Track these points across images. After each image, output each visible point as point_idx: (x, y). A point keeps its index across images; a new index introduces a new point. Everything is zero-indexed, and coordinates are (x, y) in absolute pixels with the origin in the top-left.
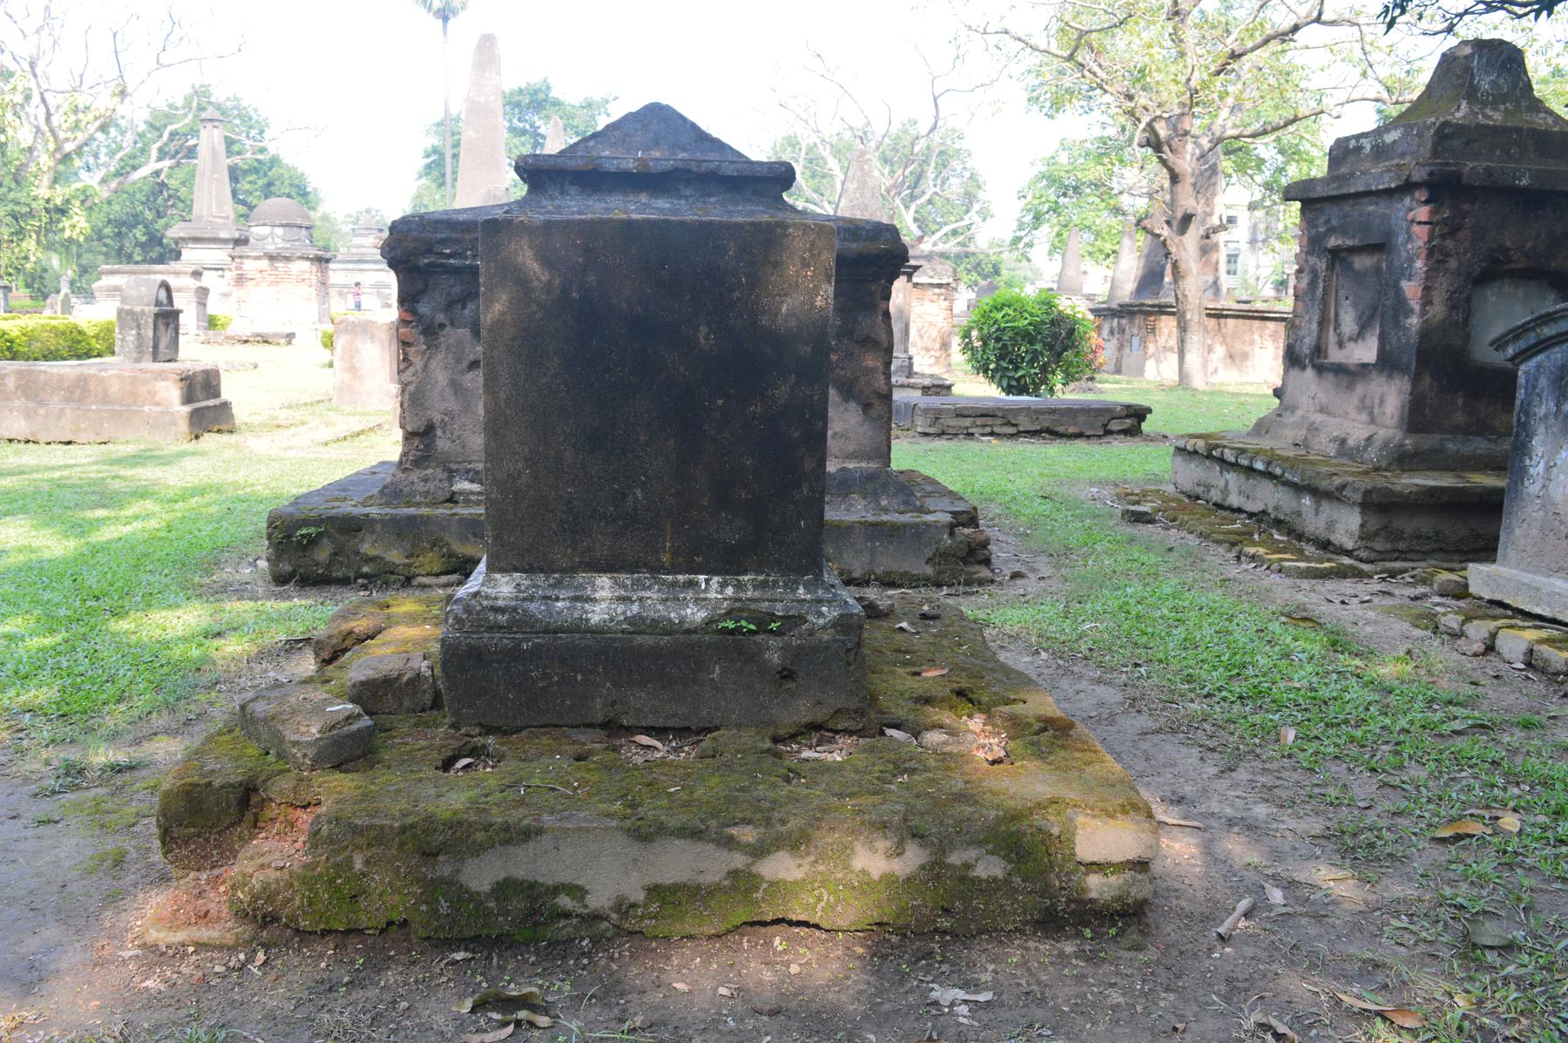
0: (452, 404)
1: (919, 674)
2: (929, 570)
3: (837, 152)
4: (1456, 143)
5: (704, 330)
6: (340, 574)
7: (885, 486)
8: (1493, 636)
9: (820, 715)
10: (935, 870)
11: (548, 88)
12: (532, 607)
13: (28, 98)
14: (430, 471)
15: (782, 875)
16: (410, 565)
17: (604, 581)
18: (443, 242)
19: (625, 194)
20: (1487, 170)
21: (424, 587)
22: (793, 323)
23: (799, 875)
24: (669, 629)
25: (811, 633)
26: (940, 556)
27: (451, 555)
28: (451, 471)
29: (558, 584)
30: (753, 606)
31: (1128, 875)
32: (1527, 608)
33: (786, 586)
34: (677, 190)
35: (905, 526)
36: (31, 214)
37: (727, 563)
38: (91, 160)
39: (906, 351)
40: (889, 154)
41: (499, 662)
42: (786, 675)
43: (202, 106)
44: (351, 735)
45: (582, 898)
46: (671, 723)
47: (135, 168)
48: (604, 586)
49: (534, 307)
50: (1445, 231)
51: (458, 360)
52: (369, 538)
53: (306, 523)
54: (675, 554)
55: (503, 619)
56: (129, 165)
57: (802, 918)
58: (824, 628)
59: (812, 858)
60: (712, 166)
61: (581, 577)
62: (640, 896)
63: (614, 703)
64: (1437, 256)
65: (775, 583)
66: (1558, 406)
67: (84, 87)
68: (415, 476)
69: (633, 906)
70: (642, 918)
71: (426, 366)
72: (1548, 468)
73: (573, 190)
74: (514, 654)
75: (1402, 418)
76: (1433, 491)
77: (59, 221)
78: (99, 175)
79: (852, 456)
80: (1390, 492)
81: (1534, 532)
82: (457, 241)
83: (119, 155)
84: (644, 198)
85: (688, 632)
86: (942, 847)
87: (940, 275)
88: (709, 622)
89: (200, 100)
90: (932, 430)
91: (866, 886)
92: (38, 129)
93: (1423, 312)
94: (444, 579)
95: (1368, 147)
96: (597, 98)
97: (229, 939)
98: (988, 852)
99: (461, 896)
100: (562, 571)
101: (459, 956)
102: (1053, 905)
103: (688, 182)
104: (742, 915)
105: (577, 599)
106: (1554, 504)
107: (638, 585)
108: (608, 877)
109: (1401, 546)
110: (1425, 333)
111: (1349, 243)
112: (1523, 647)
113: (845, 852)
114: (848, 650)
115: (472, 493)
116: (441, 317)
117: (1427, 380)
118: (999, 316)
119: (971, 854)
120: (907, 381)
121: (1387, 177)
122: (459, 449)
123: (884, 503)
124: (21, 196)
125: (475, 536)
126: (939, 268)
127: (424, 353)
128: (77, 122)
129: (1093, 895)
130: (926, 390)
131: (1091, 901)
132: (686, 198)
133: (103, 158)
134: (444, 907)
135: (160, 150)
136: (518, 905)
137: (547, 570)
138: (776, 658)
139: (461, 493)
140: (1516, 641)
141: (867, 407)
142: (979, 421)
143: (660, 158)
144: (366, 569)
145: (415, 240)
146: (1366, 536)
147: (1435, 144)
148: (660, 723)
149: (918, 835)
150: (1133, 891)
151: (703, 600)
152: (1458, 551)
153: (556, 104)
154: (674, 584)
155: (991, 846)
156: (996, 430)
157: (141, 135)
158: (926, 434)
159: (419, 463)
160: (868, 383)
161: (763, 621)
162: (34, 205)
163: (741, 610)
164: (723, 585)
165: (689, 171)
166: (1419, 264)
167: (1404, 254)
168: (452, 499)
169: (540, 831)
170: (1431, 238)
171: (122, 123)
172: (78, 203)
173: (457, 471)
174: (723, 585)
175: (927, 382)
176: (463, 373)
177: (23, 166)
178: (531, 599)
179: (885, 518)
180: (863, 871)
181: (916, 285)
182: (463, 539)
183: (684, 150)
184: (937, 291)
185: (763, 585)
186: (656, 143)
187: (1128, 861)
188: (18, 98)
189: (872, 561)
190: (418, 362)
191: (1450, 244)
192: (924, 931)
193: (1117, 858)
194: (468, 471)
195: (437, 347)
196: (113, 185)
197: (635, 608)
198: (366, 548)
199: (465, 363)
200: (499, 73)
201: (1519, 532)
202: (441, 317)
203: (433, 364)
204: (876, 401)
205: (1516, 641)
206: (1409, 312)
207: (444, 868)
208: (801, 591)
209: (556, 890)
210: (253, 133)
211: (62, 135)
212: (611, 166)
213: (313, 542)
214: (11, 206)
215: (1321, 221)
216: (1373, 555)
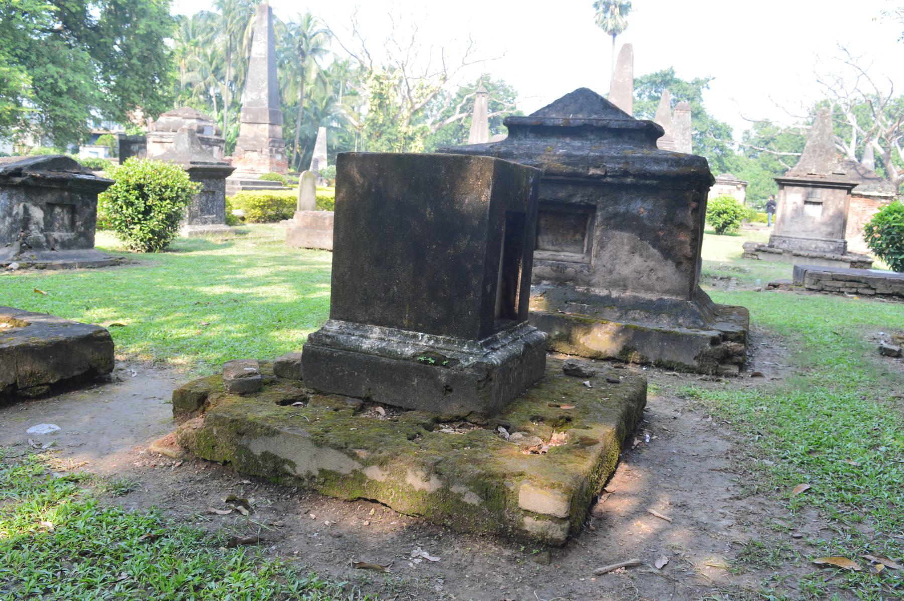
1: (559, 406)
2: (695, 364)
3: (855, 110)
5: (429, 210)
7: (684, 311)
9: (463, 412)
10: (444, 493)
11: (673, 73)
12: (341, 337)
13: (401, 82)
15: (375, 478)
17: (377, 329)
19: (558, 138)
22: (470, 209)
24: (397, 357)
26: (703, 356)
29: (357, 329)
30: (438, 351)
31: (548, 523)
33: (459, 343)
34: (586, 136)
35: (683, 335)
36: (397, 140)
37: (433, 329)
38: (429, 113)
39: (843, 238)
40: (893, 111)
42: (448, 389)
43: (487, 86)
44: (249, 382)
45: (294, 468)
46: (394, 403)
47: (449, 117)
48: (376, 332)
54: (410, 321)
55: (328, 341)
56: (447, 115)
57: (383, 502)
58: (467, 367)
59: (388, 472)
60: (605, 122)
61: (368, 326)
62: (316, 473)
63: (369, 389)
65: (454, 341)
67: (427, 77)
69: (314, 477)
70: (317, 483)
73: (531, 135)
74: (330, 358)
77: (410, 144)
78: (430, 121)
79: (667, 292)
83: (442, 110)
84: (568, 140)
85: (404, 359)
86: (448, 482)
87: (887, 191)
88: (415, 356)
89: (485, 81)
90: (814, 287)
91: (412, 493)
92: (404, 97)
96: (702, 78)
97: (174, 455)
98: (470, 490)
99: (249, 455)
100: (360, 322)
101: (245, 482)
102: (505, 528)
103: (592, 132)
104: (357, 494)
105: (362, 336)
107: (392, 334)
108: (305, 461)
113: (403, 473)
114: (479, 381)
118: (891, 218)
119: (462, 489)
120: (840, 257)
123: (680, 321)
124: (393, 130)
126: (886, 186)
128: (422, 94)
129: (528, 528)
130: (853, 264)
131: (527, 532)
132: (591, 140)
133: (435, 112)
134: (244, 460)
135: (462, 108)
136: (270, 465)
137: (354, 320)
138: (443, 379)
141: (678, 264)
142: (848, 284)
143: (581, 118)
148: (389, 402)
149: (439, 474)
150: (550, 532)
151: (414, 345)
153: (678, 82)
154: (407, 335)
155: (472, 487)
156: (860, 291)
157: (454, 100)
158: (810, 289)
160: (680, 250)
161: (439, 361)
162: (399, 135)
163: (432, 352)
164: (429, 339)
165: (592, 126)
169: (279, 433)
171: (445, 94)
172: (419, 135)
174: (429, 339)
175: (855, 259)
177: (396, 116)
178: (342, 333)
179: (677, 330)
180: (411, 485)
181: (853, 195)
183: (596, 114)
184: (884, 201)
185: (448, 342)
186: (581, 110)
187: (549, 515)
188: (396, 82)
189: (661, 354)
192: (438, 523)
193: (541, 511)
196: (437, 126)
197: (384, 344)
200: (632, 66)
204: (685, 261)
207: (244, 441)
208: (466, 347)
209: (285, 461)
210: (510, 99)
211: (415, 100)
212: (549, 123)
214: (388, 136)
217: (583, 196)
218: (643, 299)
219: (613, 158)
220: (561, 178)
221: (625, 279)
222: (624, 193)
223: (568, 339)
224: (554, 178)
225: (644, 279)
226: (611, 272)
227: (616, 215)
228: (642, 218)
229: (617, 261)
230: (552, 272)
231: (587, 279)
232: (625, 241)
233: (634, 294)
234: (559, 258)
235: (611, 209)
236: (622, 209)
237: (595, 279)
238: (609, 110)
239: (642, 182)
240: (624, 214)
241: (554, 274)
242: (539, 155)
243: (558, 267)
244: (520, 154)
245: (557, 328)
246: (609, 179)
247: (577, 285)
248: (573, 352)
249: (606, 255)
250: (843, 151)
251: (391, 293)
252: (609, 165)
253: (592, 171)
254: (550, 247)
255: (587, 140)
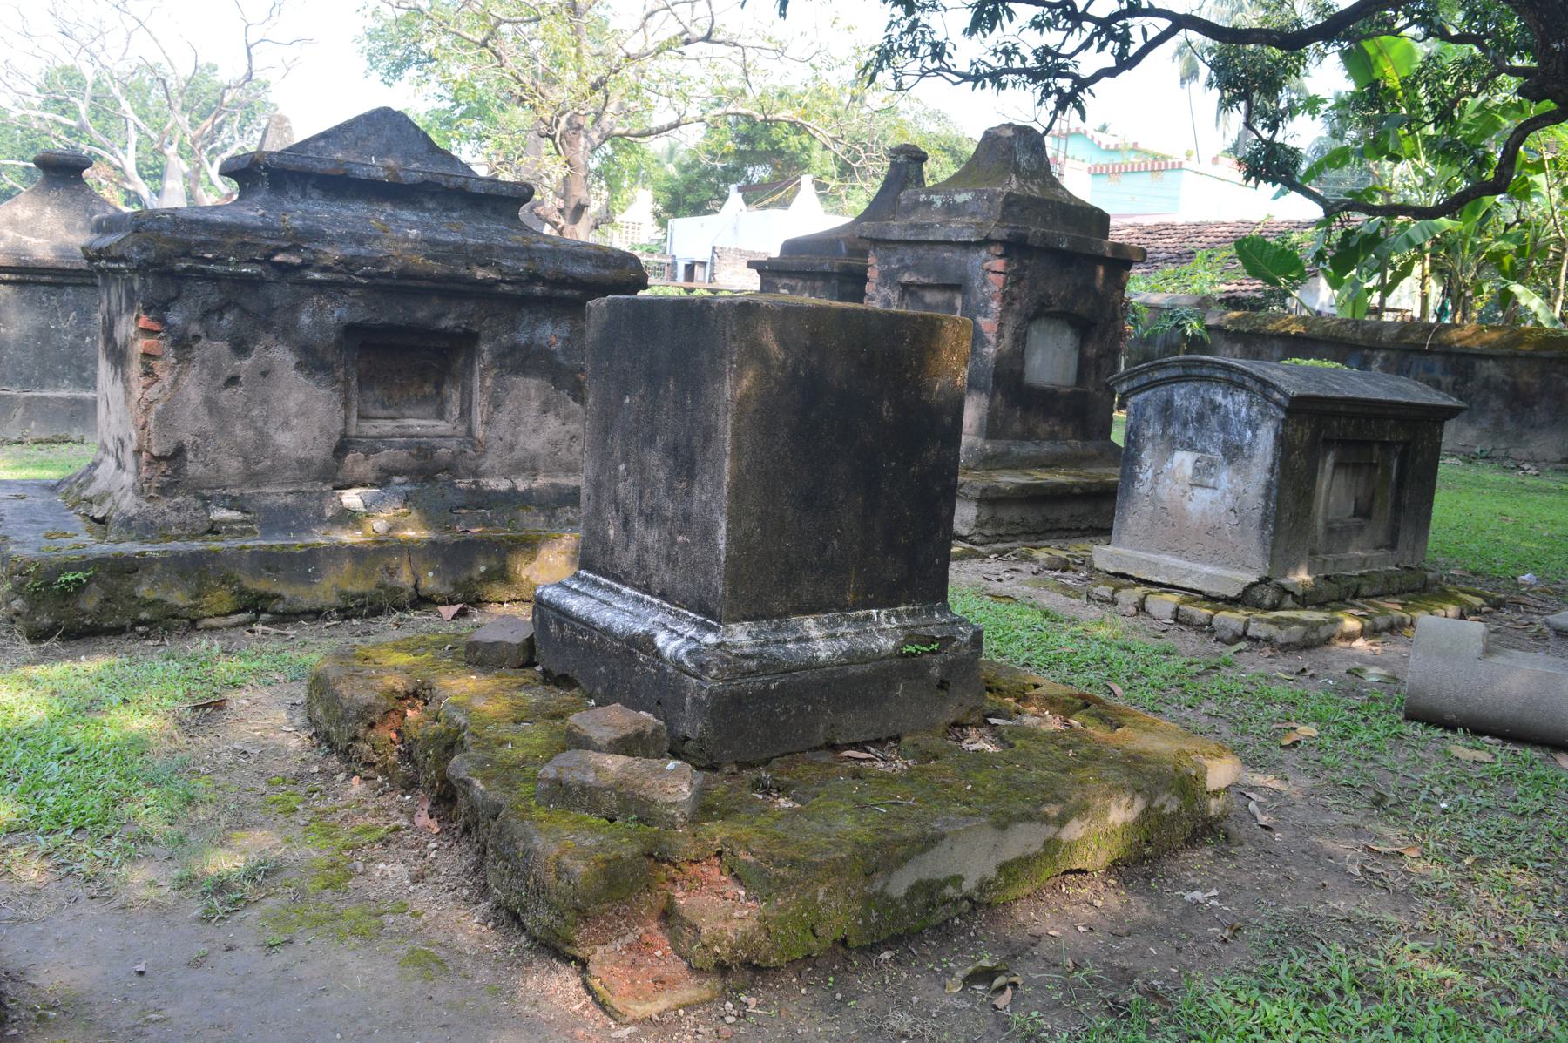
0: (207, 424)
4: (1016, 209)
5: (886, 403)
6: (112, 623)
8: (1143, 600)
14: (180, 499)
16: (195, 607)
18: (203, 245)
19: (369, 202)
20: (1043, 234)
21: (211, 629)
23: (1080, 834)
25: (957, 649)
27: (242, 592)
28: (204, 498)
32: (1149, 578)
34: (421, 203)
41: (754, 703)
42: (943, 685)
49: (773, 383)
50: (1015, 278)
51: (214, 376)
52: (147, 581)
53: (69, 567)
54: (856, 594)
55: (753, 664)
64: (1008, 300)
66: (1164, 431)
68: (164, 505)
71: (175, 382)
72: (1156, 475)
73: (315, 194)
74: (764, 695)
75: (980, 426)
76: (1024, 487)
80: (997, 489)
81: (1144, 521)
82: (217, 245)
86: (1151, 798)
93: (998, 344)
94: (233, 619)
95: (939, 203)
100: (779, 616)
103: (433, 196)
106: (1161, 501)
109: (1001, 531)
110: (999, 360)
111: (925, 281)
112: (1171, 608)
115: (235, 522)
116: (195, 328)
117: (999, 398)
121: (967, 232)
122: (213, 474)
125: (269, 569)
127: (173, 367)
132: (429, 210)
139: (222, 522)
140: (1162, 605)
144: (144, 615)
145: (169, 241)
146: (980, 524)
147: (1004, 209)
148: (862, 738)
152: (1035, 533)
159: (165, 490)
164: (888, 616)
165: (438, 185)
166: (994, 305)
167: (980, 296)
168: (213, 530)
169: (943, 837)
170: (1005, 286)
173: (211, 498)
176: (219, 389)
182: (255, 573)
183: (417, 160)
190: (166, 377)
191: (1016, 290)
194: (224, 497)
195: (190, 361)
198: (144, 591)
199: (222, 380)
201: (1133, 518)
202: (195, 328)
203: (186, 381)
205: (1162, 605)
206: (986, 342)
209: (944, 884)
212: (361, 173)
213: (79, 586)
215: (894, 259)
216: (984, 540)
217: (458, 318)
218: (567, 487)
219: (508, 249)
220: (424, 284)
221: (534, 458)
222: (525, 311)
223: (502, 575)
224: (410, 283)
225: (563, 455)
226: (511, 448)
227: (514, 348)
228: (554, 352)
229: (522, 428)
230: (411, 460)
231: (472, 465)
232: (533, 392)
233: (550, 480)
234: (412, 431)
235: (504, 338)
236: (522, 338)
237: (486, 464)
238: (438, 156)
239: (558, 292)
240: (527, 346)
241: (415, 463)
242: (377, 238)
243: (419, 449)
244: (340, 236)
245: (481, 561)
246: (508, 288)
247: (456, 477)
248: (513, 596)
249: (503, 419)
250: (116, 162)
251: (829, 553)
252: (507, 263)
253: (480, 274)
254: (380, 412)
255: (424, 210)
